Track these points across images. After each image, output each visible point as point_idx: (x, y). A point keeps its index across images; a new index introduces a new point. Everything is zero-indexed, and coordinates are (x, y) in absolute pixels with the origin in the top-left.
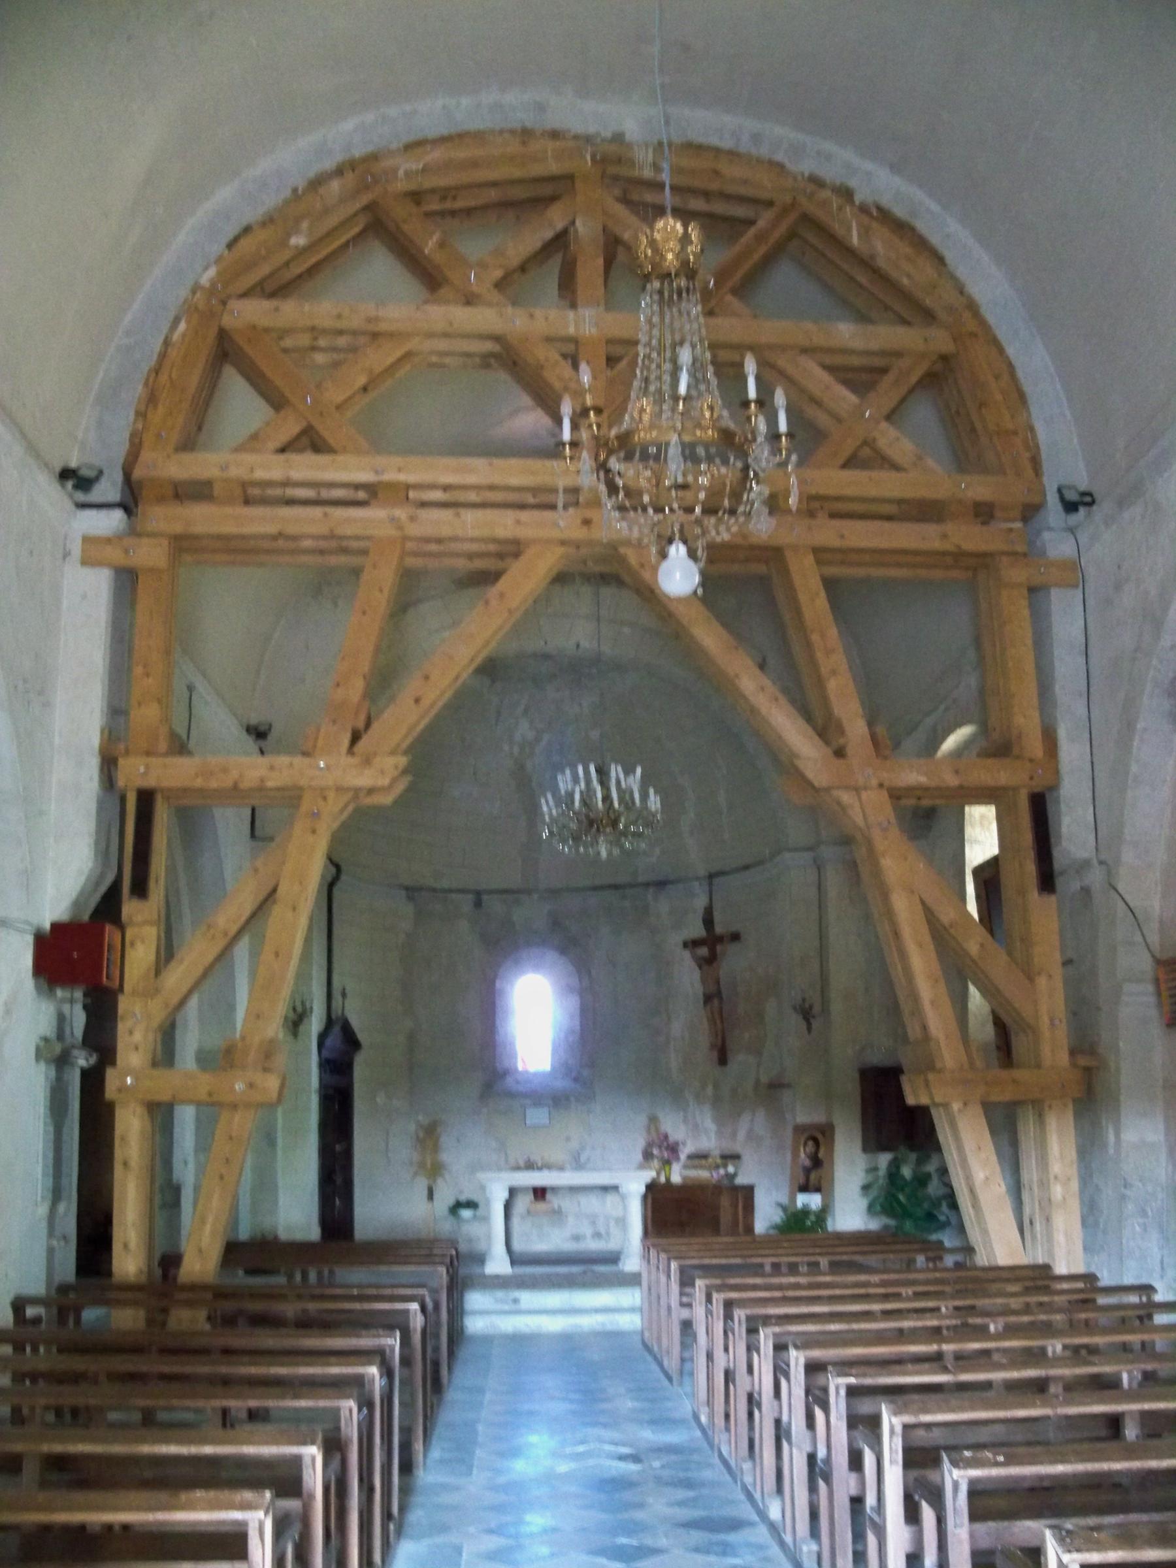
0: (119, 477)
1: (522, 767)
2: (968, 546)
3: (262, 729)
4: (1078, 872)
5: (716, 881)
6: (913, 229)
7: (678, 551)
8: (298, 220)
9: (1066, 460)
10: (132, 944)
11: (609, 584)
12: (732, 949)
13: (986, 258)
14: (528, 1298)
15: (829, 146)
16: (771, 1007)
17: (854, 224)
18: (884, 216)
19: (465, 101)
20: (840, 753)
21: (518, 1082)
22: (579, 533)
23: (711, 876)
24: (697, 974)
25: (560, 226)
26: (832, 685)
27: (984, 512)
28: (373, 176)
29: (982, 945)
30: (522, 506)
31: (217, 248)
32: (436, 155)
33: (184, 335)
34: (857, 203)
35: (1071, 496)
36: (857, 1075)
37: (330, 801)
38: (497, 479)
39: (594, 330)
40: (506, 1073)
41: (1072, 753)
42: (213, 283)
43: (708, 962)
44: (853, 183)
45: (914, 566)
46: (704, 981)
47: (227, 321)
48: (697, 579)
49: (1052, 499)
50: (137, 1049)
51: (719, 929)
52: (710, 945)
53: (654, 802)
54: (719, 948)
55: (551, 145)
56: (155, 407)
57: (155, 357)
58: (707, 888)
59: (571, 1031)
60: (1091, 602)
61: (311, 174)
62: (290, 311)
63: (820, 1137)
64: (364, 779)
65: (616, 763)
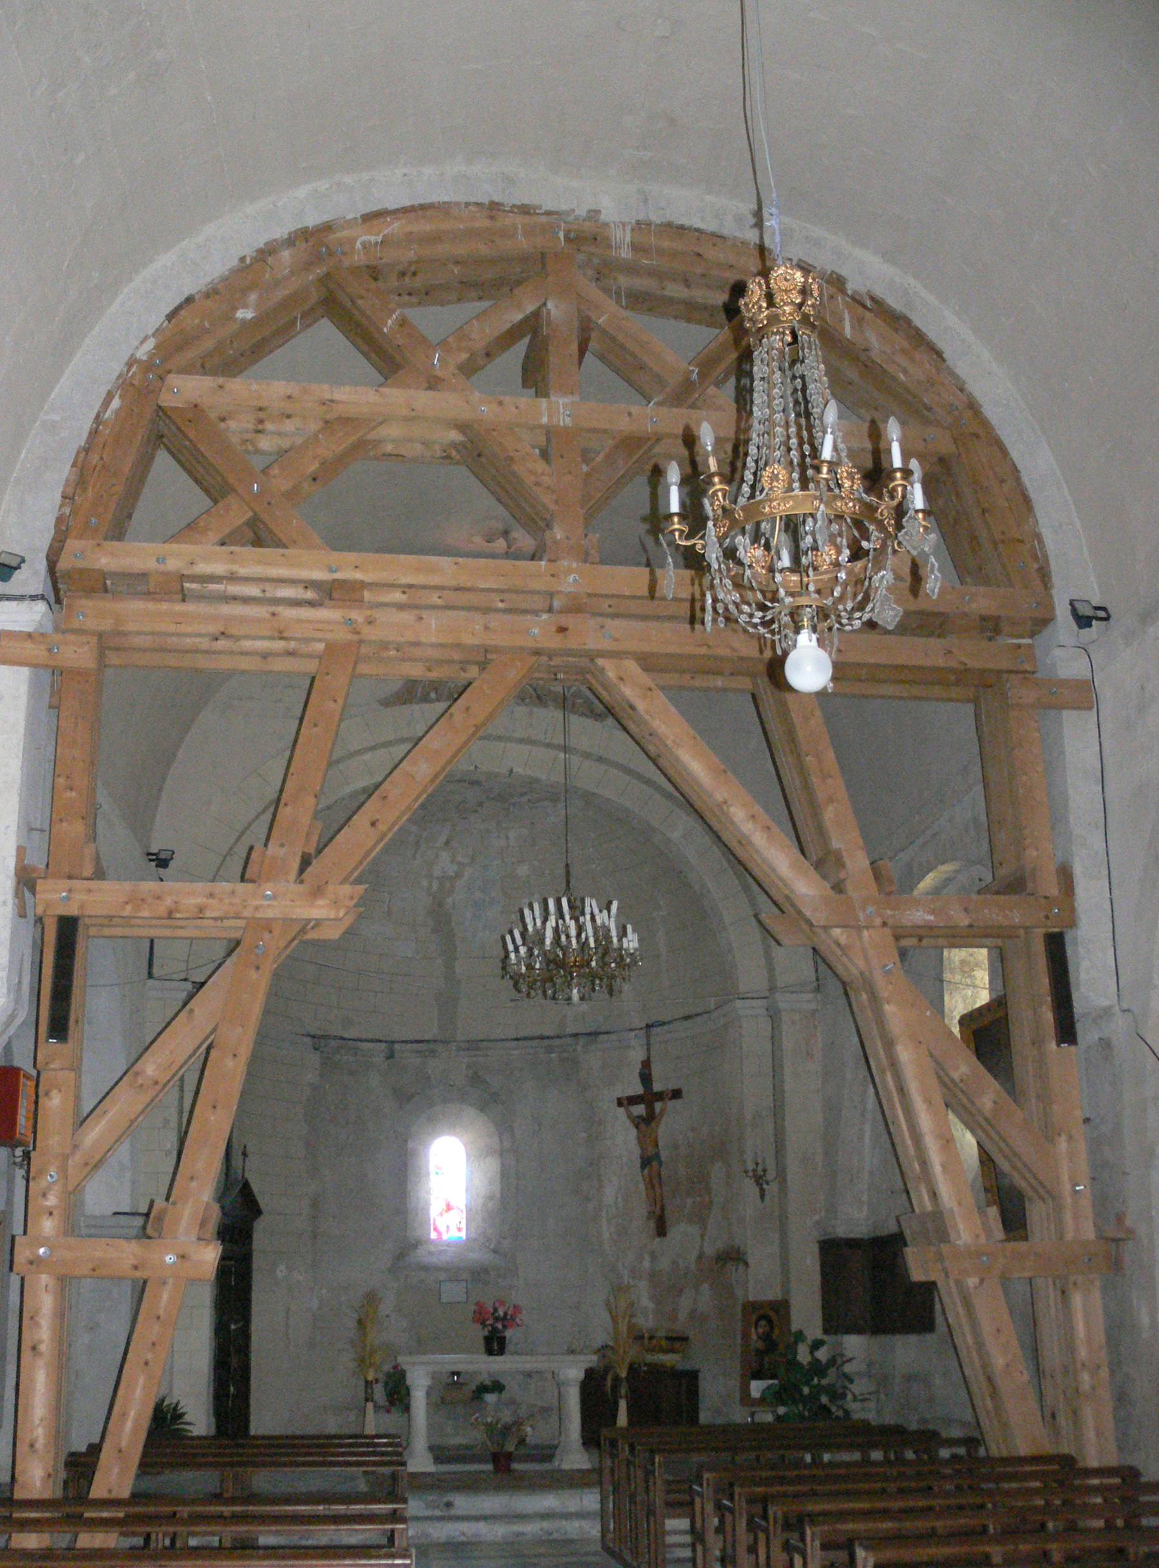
0: (42, 566)
1: (440, 905)
2: (974, 664)
3: (162, 856)
4: (1094, 1021)
5: (654, 1031)
6: (908, 322)
7: (806, 640)
8: (245, 291)
9: (1075, 576)
10: (47, 1094)
11: (546, 706)
12: (672, 1104)
13: (986, 354)
14: (463, 1503)
15: (818, 232)
16: (717, 1171)
17: (847, 316)
18: (879, 308)
19: (428, 170)
20: (839, 888)
21: (431, 1253)
22: (555, 642)
23: (648, 1026)
24: (633, 1132)
25: (530, 308)
26: (829, 814)
27: (991, 626)
28: (327, 247)
29: (995, 1103)
30: (487, 610)
31: (156, 319)
32: (395, 227)
33: (117, 412)
34: (849, 292)
35: (1088, 611)
36: (816, 1249)
37: (276, 933)
38: (465, 580)
39: (568, 421)
40: (417, 1244)
41: (1089, 893)
42: (151, 356)
43: (646, 1123)
44: (844, 272)
45: (912, 682)
46: (641, 1140)
47: (166, 400)
48: (828, 672)
49: (1062, 612)
50: (51, 1214)
51: (657, 1087)
52: (647, 1104)
53: (631, 942)
54: (658, 1106)
55: (519, 220)
56: (85, 490)
57: (85, 435)
58: (644, 1041)
59: (491, 1198)
60: (1107, 727)
61: (260, 243)
62: (242, 388)
63: (771, 1314)
64: (319, 910)
65: (592, 897)
